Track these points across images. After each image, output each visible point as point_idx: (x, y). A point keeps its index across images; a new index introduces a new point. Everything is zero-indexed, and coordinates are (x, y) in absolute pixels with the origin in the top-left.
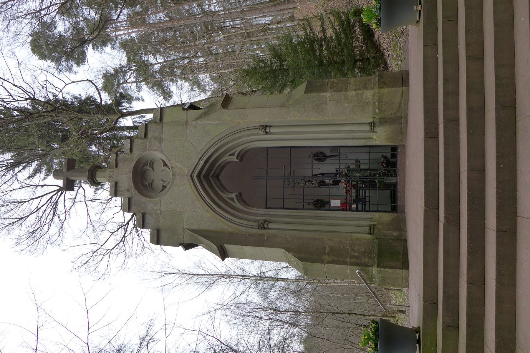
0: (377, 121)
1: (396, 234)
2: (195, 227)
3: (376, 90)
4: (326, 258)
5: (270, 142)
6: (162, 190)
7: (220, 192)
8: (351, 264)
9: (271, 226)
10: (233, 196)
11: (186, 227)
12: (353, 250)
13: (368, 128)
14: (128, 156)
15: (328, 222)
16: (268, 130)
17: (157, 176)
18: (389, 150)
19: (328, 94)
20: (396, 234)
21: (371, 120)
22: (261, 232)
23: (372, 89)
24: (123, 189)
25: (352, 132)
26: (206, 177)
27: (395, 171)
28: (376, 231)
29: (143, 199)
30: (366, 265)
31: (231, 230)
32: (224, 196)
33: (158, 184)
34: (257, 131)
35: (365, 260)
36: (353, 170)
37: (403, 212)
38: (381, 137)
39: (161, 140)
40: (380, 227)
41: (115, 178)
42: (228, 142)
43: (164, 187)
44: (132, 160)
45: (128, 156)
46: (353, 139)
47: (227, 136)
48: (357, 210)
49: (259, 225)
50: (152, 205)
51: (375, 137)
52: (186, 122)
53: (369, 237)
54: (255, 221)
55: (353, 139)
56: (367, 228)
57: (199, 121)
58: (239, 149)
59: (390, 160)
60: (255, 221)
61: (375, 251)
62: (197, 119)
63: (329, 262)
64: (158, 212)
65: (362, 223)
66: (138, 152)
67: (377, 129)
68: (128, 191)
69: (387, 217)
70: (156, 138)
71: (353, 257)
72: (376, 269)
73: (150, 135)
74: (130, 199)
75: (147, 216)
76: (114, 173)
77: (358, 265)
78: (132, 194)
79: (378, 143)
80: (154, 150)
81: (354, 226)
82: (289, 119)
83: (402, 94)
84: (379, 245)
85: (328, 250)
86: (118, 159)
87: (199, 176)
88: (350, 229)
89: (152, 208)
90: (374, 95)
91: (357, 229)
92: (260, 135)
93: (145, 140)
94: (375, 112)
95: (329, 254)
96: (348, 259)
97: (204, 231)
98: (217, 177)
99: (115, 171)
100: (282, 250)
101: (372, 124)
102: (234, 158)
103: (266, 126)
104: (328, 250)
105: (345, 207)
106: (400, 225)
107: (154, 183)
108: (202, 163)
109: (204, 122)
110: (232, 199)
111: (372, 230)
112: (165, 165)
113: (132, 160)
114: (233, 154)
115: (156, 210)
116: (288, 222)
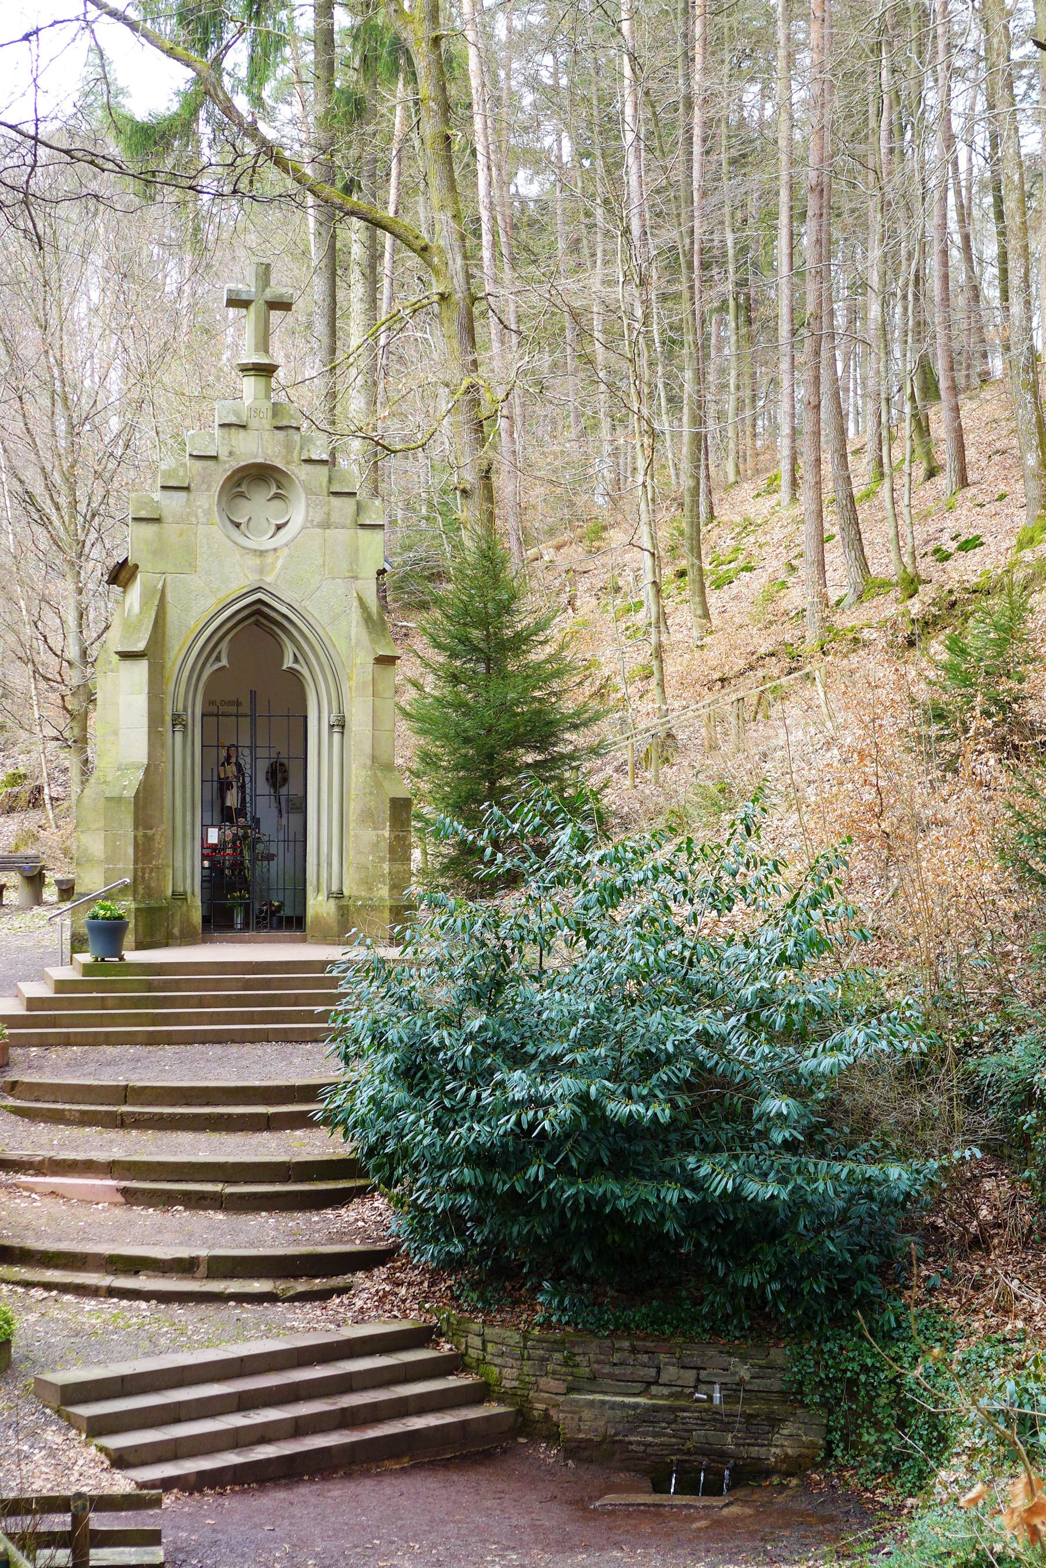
0: (344, 902)
1: (176, 931)
2: (169, 597)
3: (388, 903)
4: (140, 833)
5: (316, 728)
6: (232, 521)
7: (229, 637)
8: (135, 870)
9: (179, 736)
10: (224, 662)
11: (169, 577)
12: (151, 870)
13: (335, 888)
14: (296, 454)
15: (189, 828)
16: (336, 729)
17: (259, 506)
18: (298, 913)
19: (387, 834)
20: (176, 931)
21: (346, 893)
22: (168, 719)
23: (391, 896)
24: (234, 443)
25: (330, 865)
26: (259, 612)
27: (265, 927)
28: (179, 903)
29: (216, 487)
30: (135, 892)
31: (169, 664)
32: (224, 645)
33: (245, 511)
34: (335, 710)
35: (141, 889)
36: (254, 848)
37: (204, 942)
38: (318, 905)
39: (326, 525)
40: (184, 908)
41: (254, 423)
42: (312, 648)
43: (238, 525)
44: (288, 463)
45: (296, 454)
46: (318, 865)
47: (329, 657)
48: (203, 868)
49: (179, 716)
50: (206, 506)
51: (320, 898)
52: (356, 578)
53: (169, 893)
54: (185, 709)
55: (318, 865)
56: (181, 890)
57: (356, 603)
58: (305, 671)
59: (292, 922)
60: (185, 709)
61: (153, 904)
62: (360, 599)
63: (135, 837)
64: (193, 520)
65: (189, 881)
66: (303, 477)
67: (332, 902)
68: (231, 453)
69: (197, 917)
70: (328, 514)
71: (143, 869)
72: (133, 906)
73: (335, 501)
74: (215, 458)
75: (183, 495)
76: (264, 421)
77: (135, 880)
78: (225, 462)
79: (311, 901)
80: (307, 512)
81: (185, 873)
82: (354, 766)
83: (924, 199)
84: (161, 908)
85: (150, 832)
86: (291, 431)
87: (260, 601)
88: (179, 864)
89: (200, 507)
90: (381, 899)
91: (179, 874)
92: (330, 713)
93: (325, 493)
94: (357, 899)
95: (145, 835)
96: (140, 865)
97: (164, 619)
98: (257, 623)
99: (267, 423)
100: (145, 761)
101: (340, 895)
102: (288, 663)
103: (343, 727)
104: (150, 832)
105: (211, 852)
106: (188, 939)
107: (245, 501)
108: (284, 610)
109: (355, 615)
110: (218, 659)
111: (179, 896)
112: (279, 527)
113: (288, 463)
114: (296, 660)
115: (196, 516)
116: (185, 756)
